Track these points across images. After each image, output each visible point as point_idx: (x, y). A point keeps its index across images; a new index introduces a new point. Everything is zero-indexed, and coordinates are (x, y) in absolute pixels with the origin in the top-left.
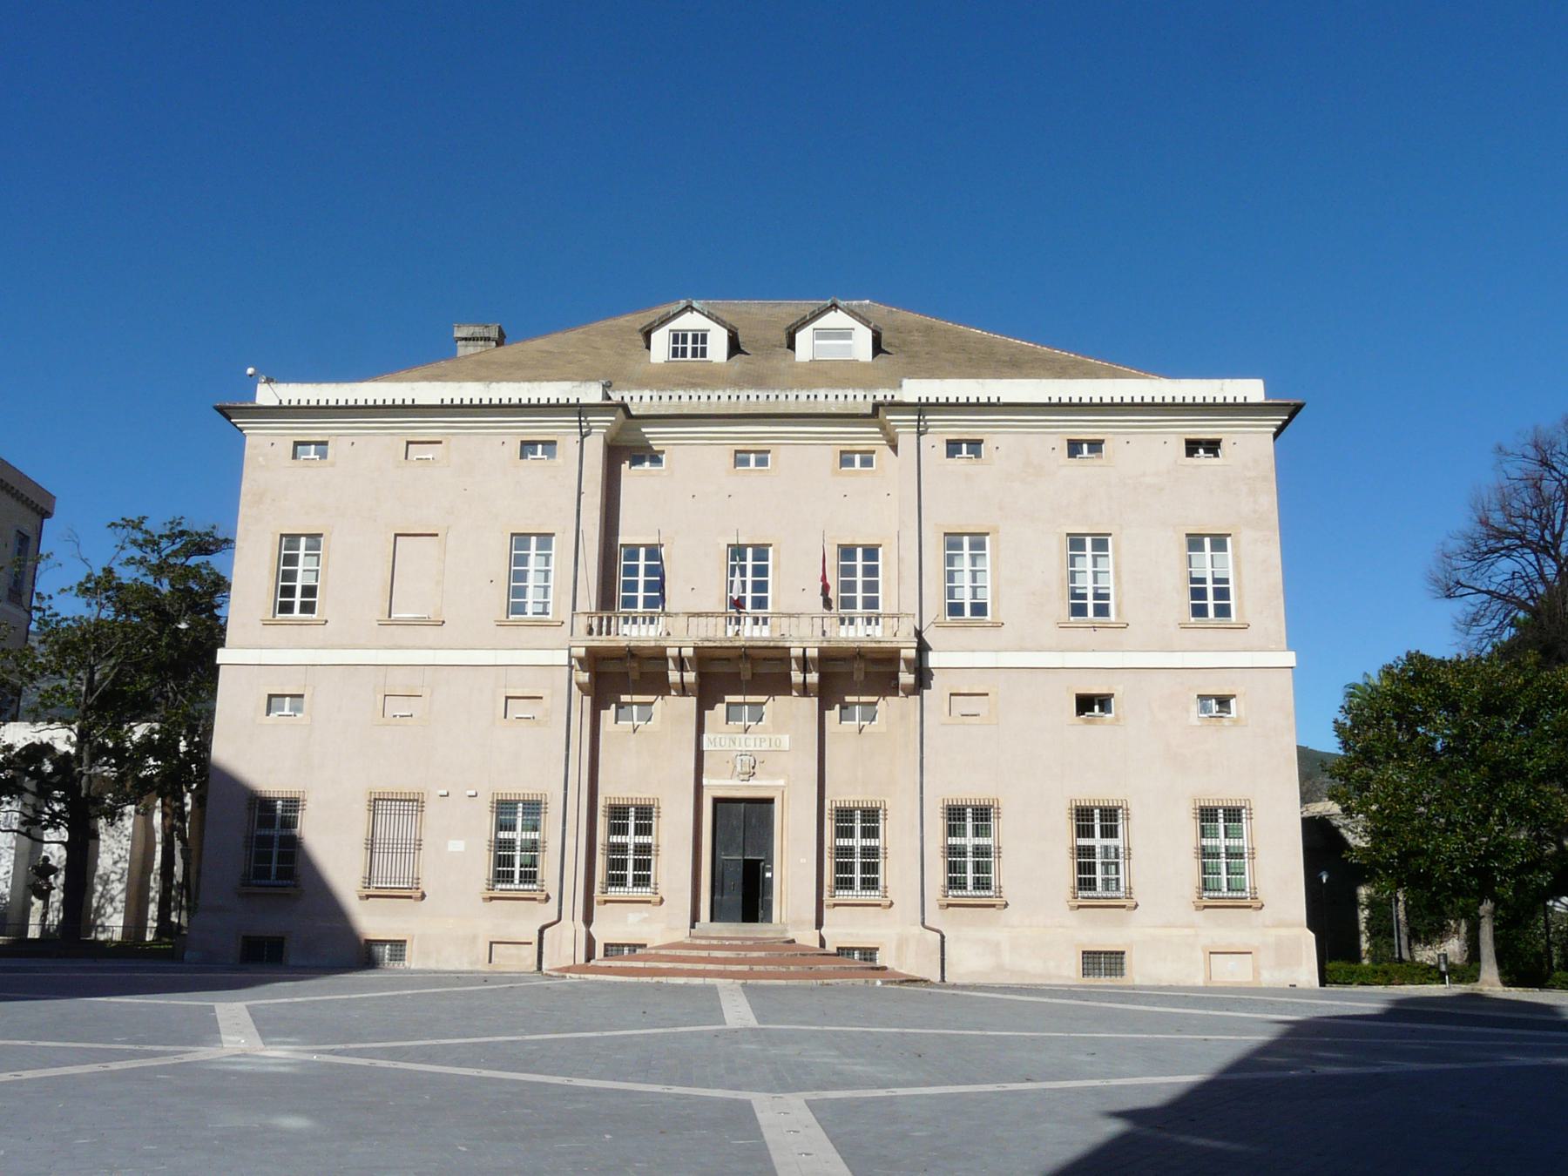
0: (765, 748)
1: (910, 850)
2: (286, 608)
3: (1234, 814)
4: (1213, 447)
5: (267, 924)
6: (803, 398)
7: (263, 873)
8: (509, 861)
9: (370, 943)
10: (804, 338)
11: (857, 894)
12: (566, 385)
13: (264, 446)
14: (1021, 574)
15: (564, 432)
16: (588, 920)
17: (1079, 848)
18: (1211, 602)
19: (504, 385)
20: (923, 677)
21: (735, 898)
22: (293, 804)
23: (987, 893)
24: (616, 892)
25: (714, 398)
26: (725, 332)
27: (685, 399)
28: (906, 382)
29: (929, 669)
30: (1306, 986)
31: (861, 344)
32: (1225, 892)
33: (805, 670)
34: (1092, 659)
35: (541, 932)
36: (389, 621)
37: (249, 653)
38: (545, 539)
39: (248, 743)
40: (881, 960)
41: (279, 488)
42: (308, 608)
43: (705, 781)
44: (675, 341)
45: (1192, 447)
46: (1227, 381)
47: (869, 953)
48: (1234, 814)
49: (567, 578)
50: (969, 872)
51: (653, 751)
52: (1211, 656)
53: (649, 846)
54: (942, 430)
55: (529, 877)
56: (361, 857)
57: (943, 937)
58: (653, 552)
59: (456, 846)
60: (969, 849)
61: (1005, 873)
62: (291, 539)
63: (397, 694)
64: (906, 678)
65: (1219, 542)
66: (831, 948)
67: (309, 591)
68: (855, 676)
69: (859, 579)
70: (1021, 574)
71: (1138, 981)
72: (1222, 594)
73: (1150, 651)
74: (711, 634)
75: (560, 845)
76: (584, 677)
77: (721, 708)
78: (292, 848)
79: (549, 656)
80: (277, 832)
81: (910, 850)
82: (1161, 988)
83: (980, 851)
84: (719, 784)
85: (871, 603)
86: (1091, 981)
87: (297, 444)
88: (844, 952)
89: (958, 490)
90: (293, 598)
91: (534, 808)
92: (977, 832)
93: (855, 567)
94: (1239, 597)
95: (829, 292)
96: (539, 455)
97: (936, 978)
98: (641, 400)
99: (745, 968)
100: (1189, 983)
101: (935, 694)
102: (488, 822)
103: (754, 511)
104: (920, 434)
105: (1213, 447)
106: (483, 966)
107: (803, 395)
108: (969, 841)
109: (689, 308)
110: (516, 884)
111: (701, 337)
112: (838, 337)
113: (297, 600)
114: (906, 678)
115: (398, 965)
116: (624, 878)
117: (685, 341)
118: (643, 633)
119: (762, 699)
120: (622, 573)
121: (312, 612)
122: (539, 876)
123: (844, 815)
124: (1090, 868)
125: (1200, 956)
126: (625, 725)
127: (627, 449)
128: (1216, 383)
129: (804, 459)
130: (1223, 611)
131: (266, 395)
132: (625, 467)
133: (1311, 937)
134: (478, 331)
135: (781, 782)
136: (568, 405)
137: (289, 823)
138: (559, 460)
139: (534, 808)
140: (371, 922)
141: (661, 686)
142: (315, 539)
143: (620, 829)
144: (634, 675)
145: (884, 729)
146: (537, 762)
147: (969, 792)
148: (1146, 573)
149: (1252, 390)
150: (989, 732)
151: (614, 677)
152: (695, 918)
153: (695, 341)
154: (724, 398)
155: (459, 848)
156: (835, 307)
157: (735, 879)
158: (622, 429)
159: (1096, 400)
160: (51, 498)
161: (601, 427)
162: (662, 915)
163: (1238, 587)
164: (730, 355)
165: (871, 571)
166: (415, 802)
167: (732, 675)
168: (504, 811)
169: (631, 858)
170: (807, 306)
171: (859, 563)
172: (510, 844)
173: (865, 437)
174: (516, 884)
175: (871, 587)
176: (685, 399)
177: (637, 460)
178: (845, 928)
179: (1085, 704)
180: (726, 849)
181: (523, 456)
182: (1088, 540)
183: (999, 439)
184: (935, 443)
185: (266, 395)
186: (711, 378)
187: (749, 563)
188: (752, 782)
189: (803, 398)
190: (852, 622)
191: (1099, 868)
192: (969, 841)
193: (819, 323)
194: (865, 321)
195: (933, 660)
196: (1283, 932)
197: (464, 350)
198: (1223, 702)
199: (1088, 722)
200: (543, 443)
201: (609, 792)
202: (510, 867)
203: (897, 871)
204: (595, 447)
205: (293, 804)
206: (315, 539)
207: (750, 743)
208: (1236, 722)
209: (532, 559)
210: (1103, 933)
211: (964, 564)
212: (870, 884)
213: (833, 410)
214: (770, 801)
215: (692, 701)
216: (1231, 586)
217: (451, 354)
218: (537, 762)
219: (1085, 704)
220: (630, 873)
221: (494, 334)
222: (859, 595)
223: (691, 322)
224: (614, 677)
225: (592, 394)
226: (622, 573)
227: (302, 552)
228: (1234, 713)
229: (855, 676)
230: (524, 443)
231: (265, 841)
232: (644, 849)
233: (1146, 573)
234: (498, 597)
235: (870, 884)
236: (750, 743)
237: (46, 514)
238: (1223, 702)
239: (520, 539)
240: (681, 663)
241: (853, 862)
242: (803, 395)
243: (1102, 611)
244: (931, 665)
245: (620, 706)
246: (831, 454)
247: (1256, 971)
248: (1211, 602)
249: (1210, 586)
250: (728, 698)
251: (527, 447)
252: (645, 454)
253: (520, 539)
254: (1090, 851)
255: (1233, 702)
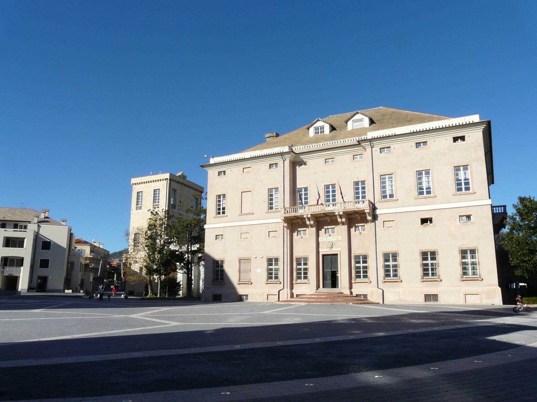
0: (334, 240)
1: (375, 266)
2: (219, 213)
3: (473, 252)
4: (463, 138)
5: (218, 292)
6: (342, 142)
7: (217, 279)
8: (271, 274)
9: (241, 296)
10: (350, 123)
11: (362, 279)
12: (280, 148)
13: (212, 173)
14: (404, 184)
15: (279, 160)
16: (292, 288)
17: (386, 265)
18: (463, 186)
19: (265, 150)
20: (375, 217)
21: (329, 282)
22: (222, 262)
23: (428, 277)
24: (358, 280)
25: (319, 145)
26: (328, 125)
27: (311, 147)
28: (368, 133)
29: (377, 215)
30: (498, 304)
31: (366, 121)
32: (470, 276)
33: (341, 218)
34: (425, 208)
35: (279, 292)
36: (241, 214)
37: (212, 225)
38: (277, 189)
39: (213, 248)
40: (369, 298)
41: (215, 184)
42: (224, 213)
43: (320, 250)
44: (316, 130)
45: (455, 139)
46: (467, 117)
47: (365, 296)
48: (473, 252)
49: (282, 199)
50: (391, 271)
51: (305, 243)
52: (464, 203)
53: (367, 266)
54: (378, 146)
55: (276, 278)
56: (238, 274)
57: (383, 291)
58: (306, 189)
59: (259, 270)
60: (430, 264)
61: (401, 272)
62: (219, 196)
63: (243, 233)
64: (369, 218)
65: (465, 167)
66: (354, 295)
67: (224, 209)
68: (354, 219)
69: (360, 191)
70: (404, 184)
71: (442, 303)
72: (467, 183)
73: (444, 203)
74: (315, 211)
75: (283, 268)
76: (286, 225)
77: (323, 230)
78: (223, 271)
79: (277, 220)
80: (219, 269)
81: (375, 266)
82: (448, 305)
83: (432, 265)
84: (324, 250)
85: (334, 200)
86: (427, 303)
87: (381, 149)
88: (357, 296)
89: (384, 162)
90: (221, 211)
91: (277, 260)
92: (472, 257)
93: (359, 187)
94: (472, 184)
95: (355, 107)
96: (422, 146)
97: (381, 302)
98: (298, 149)
99: (315, 300)
100: (458, 304)
101: (379, 222)
102: (266, 264)
103: (333, 173)
104: (372, 148)
105: (463, 138)
106: (266, 301)
107: (342, 141)
108: (391, 263)
109: (318, 120)
110: (392, 277)
111: (322, 128)
112: (360, 121)
113: (221, 211)
114: (369, 218)
115: (247, 301)
116: (272, 277)
117: (318, 129)
118: (361, 206)
119: (334, 227)
120: (296, 195)
121: (393, 197)
122: (398, 275)
123: (357, 257)
124: (427, 270)
125: (462, 296)
126: (357, 232)
127: (296, 163)
128: (463, 118)
129: (343, 158)
130: (467, 189)
131: (212, 161)
132: (297, 167)
133: (500, 289)
134: (271, 135)
135: (340, 249)
136: (278, 153)
137: (222, 266)
138: (279, 168)
139: (277, 260)
140: (241, 290)
141: (336, 223)
142: (224, 196)
143: (359, 262)
144: (329, 221)
145: (367, 232)
146: (276, 248)
147: (390, 249)
148: (442, 180)
149: (476, 118)
150: (396, 233)
151: (294, 224)
152: (318, 287)
153: (321, 129)
154: (321, 145)
155: (259, 271)
156: (357, 113)
157: (329, 277)
158: (295, 157)
159: (379, 137)
160: (203, 188)
161: (288, 158)
162: (307, 288)
163: (472, 181)
164: (370, 125)
165: (363, 188)
166: (248, 260)
167: (323, 221)
168: (270, 261)
169: (302, 272)
170: (349, 115)
171: (360, 186)
172: (271, 269)
173: (358, 150)
174: (392, 277)
175: (364, 192)
176: (311, 147)
177: (300, 165)
178: (358, 289)
179: (424, 221)
180: (327, 268)
181: (270, 168)
182: (424, 172)
183: (396, 146)
184: (376, 149)
185: (212, 161)
186: (325, 139)
187: (331, 190)
188: (332, 250)
189: (342, 142)
190: (359, 203)
191: (430, 270)
192: (391, 263)
193: (354, 118)
194: (366, 116)
195: (378, 212)
196: (490, 288)
197: (268, 140)
198: (468, 217)
199: (425, 226)
200: (423, 142)
201: (296, 255)
202: (271, 275)
203: (371, 273)
204: (287, 163)
205: (222, 262)
206: (224, 196)
207: (331, 239)
208: (472, 223)
209: (387, 182)
210: (431, 289)
211: (424, 179)
212: (365, 277)
213: (349, 144)
214: (337, 255)
215: (345, 227)
216: (470, 181)
217: (265, 141)
218: (276, 248)
219: (424, 221)
220: (362, 274)
221: (275, 135)
222: (360, 195)
223: (319, 124)
224: (294, 224)
225: (286, 149)
226: (296, 195)
227: (274, 193)
228: (472, 220)
229: (354, 219)
230: (417, 143)
231: (216, 270)
232: (306, 269)
233: (442, 180)
234: (266, 205)
235: (365, 277)
236: (331, 239)
237: (202, 192)
238: (468, 217)
239: (420, 173)
240: (341, 217)
241: (359, 271)
242: (342, 141)
243: (429, 193)
244: (377, 213)
245: (356, 227)
246: (350, 156)
247: (481, 300)
248: (463, 186)
249: (463, 182)
250: (325, 227)
251: (271, 166)
252: (302, 163)
253: (420, 173)
254: (427, 265)
255: (471, 217)
